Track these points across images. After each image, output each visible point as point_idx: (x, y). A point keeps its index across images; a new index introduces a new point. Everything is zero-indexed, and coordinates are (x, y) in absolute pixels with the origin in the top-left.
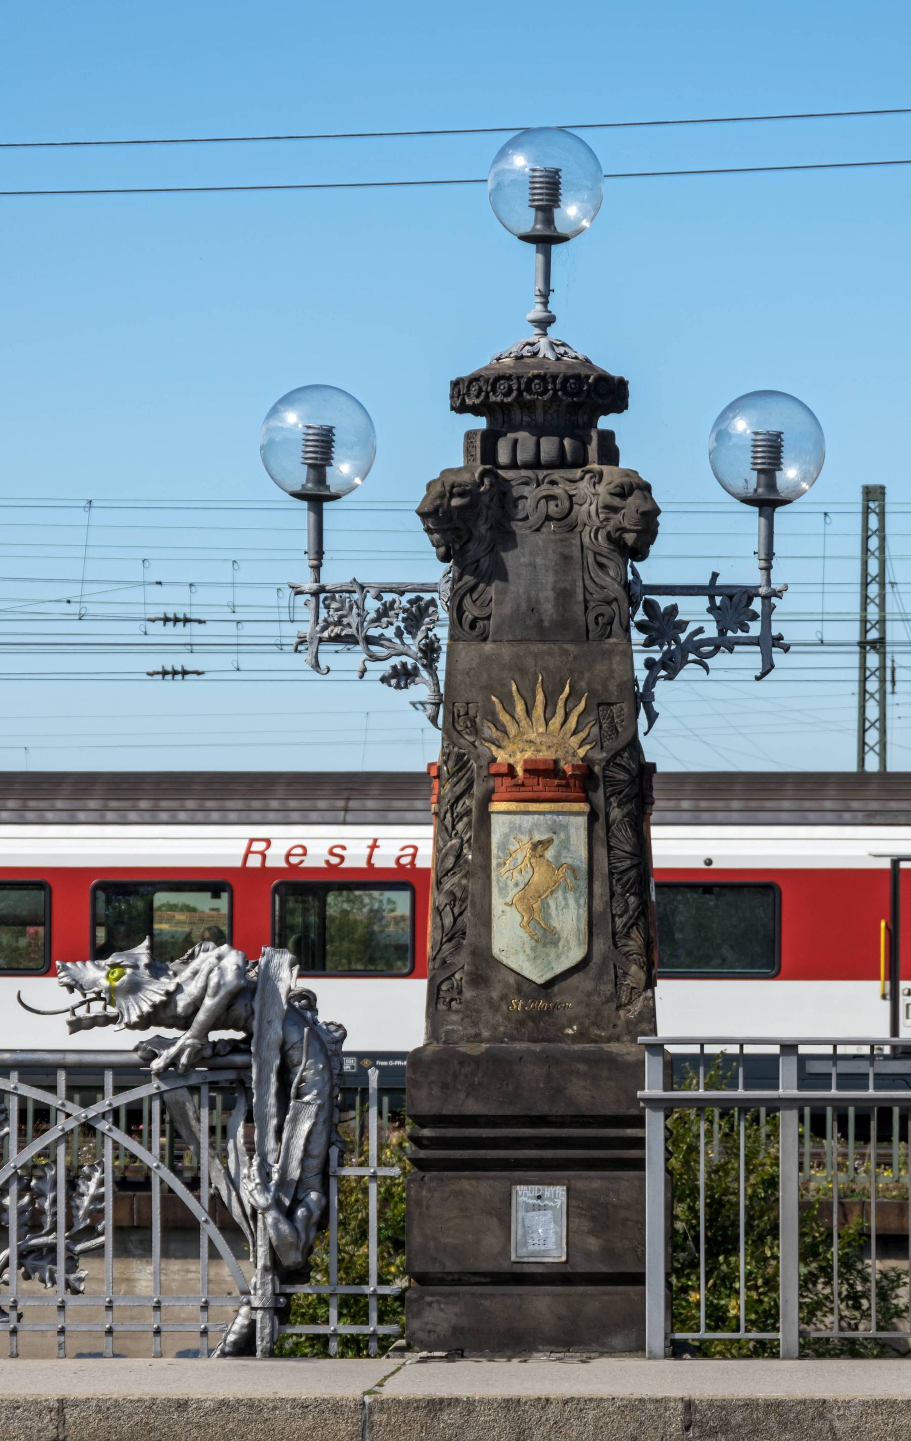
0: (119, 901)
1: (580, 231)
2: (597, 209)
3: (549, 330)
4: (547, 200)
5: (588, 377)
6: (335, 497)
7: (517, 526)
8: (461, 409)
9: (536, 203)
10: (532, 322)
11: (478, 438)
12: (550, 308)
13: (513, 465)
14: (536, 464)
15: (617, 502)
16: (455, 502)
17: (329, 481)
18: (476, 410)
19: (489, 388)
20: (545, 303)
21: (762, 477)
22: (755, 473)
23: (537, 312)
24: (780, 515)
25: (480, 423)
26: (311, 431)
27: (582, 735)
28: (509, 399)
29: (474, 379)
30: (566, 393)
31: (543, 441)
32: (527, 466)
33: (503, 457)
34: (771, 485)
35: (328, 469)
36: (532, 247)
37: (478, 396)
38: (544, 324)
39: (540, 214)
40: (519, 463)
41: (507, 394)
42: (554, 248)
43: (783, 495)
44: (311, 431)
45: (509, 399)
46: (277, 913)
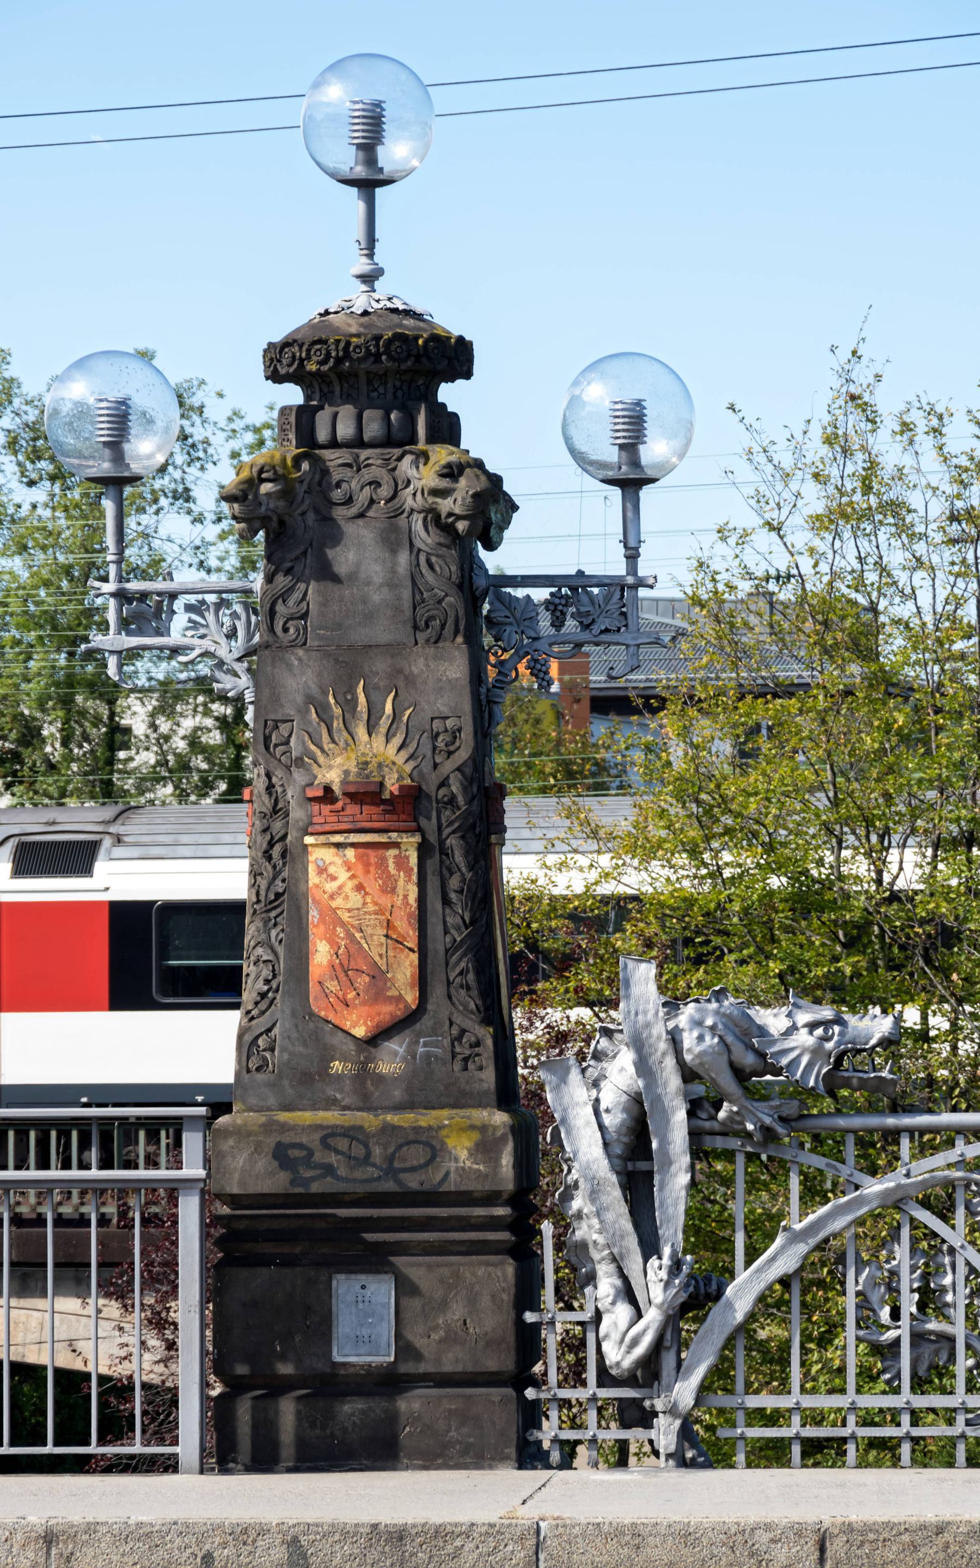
0: (934, 889)
1: (413, 170)
2: (427, 147)
3: (377, 284)
4: (363, 137)
5: (416, 338)
6: (653, 481)
7: (340, 513)
8: (275, 377)
9: (356, 141)
10: (358, 277)
11: (294, 413)
12: (376, 258)
13: (334, 444)
14: (359, 442)
15: (444, 483)
16: (266, 488)
17: (644, 462)
18: (296, 378)
19: (304, 355)
20: (371, 255)
21: (623, 453)
22: (617, 448)
23: (363, 265)
24: (646, 493)
25: (293, 395)
26: (619, 406)
27: (411, 749)
28: (325, 368)
29: (286, 344)
30: (390, 358)
31: (366, 414)
32: (348, 445)
33: (322, 435)
34: (635, 463)
35: (641, 447)
36: (354, 191)
37: (290, 365)
38: (369, 279)
39: (361, 154)
40: (339, 438)
41: (324, 362)
42: (379, 191)
43: (650, 473)
44: (619, 406)
45: (325, 368)
46: (498, 932)
